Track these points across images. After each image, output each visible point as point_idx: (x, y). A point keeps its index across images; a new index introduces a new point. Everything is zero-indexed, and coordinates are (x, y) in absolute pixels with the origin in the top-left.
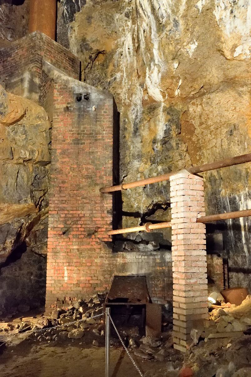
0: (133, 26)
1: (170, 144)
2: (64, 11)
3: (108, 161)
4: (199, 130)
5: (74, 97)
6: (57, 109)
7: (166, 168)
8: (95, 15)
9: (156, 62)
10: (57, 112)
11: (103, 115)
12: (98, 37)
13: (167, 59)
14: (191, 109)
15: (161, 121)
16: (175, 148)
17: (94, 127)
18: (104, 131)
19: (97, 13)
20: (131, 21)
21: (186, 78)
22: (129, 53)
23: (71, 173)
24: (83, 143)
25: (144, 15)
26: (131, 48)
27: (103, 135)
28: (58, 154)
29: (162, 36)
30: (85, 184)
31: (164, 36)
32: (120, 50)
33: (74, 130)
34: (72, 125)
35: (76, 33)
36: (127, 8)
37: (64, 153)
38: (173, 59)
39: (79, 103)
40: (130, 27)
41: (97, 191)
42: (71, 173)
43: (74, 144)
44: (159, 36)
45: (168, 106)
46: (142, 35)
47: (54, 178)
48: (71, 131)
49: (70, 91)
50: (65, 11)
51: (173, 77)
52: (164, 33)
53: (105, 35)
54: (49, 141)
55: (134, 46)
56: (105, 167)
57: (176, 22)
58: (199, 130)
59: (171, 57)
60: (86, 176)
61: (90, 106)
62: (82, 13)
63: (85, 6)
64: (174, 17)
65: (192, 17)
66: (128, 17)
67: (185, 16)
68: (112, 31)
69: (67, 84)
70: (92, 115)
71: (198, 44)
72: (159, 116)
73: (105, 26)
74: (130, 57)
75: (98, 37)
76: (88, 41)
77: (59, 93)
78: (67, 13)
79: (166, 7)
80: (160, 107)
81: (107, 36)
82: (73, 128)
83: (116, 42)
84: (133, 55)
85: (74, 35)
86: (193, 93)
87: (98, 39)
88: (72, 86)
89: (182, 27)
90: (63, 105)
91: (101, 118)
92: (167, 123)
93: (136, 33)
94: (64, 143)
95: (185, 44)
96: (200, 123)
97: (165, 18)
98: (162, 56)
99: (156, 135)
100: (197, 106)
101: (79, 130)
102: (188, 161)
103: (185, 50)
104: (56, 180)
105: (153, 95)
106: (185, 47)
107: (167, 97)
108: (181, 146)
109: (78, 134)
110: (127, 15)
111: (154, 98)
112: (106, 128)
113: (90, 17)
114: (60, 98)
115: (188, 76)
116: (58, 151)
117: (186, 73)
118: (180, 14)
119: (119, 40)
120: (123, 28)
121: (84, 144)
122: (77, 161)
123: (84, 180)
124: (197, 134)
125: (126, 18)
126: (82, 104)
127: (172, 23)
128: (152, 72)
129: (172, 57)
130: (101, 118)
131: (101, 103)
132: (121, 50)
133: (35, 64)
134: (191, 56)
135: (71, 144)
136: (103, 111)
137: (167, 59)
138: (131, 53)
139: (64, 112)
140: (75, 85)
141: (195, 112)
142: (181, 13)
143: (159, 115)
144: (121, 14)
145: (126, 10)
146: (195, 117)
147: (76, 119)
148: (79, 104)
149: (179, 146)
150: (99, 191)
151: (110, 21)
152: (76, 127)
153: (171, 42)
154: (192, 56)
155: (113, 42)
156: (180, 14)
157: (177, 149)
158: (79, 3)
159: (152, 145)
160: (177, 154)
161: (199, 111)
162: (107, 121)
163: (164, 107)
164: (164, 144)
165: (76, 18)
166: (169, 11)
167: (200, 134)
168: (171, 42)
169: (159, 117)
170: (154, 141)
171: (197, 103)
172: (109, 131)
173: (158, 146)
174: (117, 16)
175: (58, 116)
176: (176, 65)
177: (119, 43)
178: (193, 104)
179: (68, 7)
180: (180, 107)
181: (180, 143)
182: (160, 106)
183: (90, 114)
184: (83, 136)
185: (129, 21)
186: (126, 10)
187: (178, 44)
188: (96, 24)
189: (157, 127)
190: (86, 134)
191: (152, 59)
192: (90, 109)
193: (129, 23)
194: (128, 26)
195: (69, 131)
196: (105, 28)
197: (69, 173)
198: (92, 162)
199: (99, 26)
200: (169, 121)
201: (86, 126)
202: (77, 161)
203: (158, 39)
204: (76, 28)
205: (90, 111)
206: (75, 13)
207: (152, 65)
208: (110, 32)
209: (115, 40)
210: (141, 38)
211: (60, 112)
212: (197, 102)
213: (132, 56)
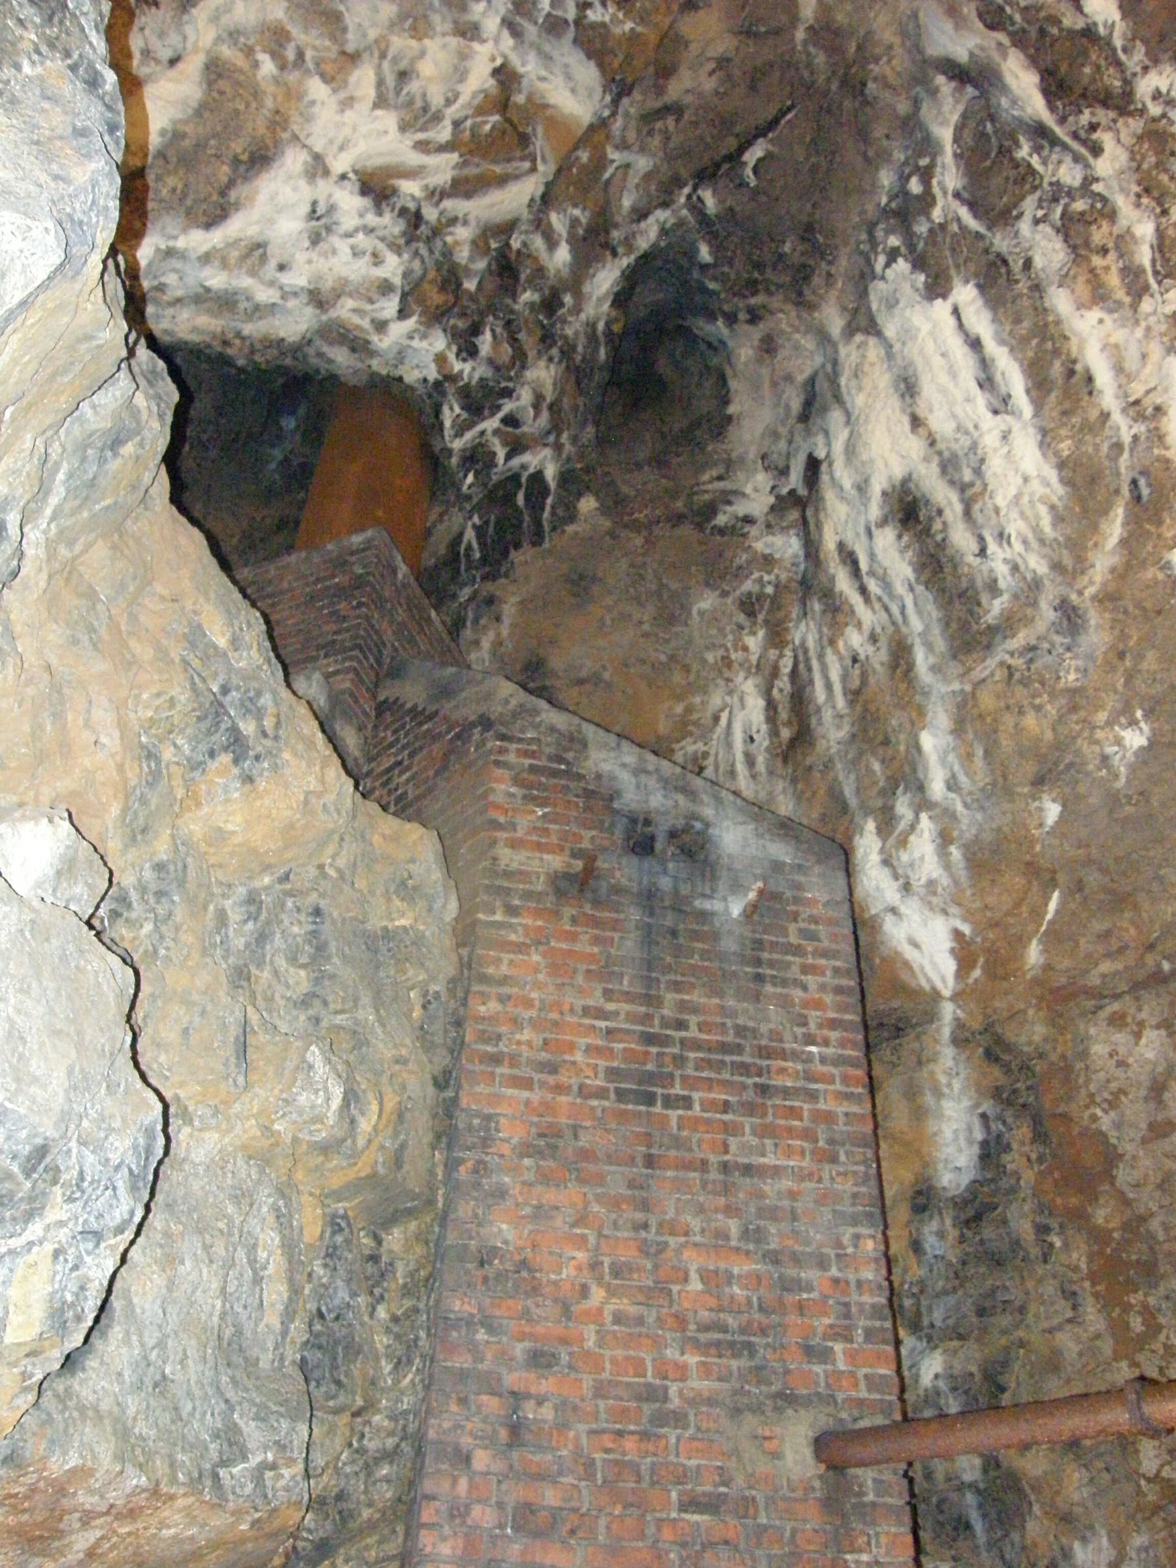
0: (773, 654)
1: (1005, 1222)
2: (461, 535)
3: (857, 1237)
4: (1146, 1162)
5: (613, 825)
6: (508, 874)
7: (973, 1369)
8: (614, 571)
9: (937, 788)
10: (508, 892)
11: (798, 951)
12: (604, 667)
13: (1005, 778)
14: (1099, 1049)
15: (946, 1090)
16: (1035, 1252)
17: (745, 1012)
18: (810, 1040)
19: (624, 564)
20: (761, 633)
21: (1080, 886)
22: (750, 761)
23: (597, 1295)
24: (679, 1098)
25: (856, 599)
26: (763, 740)
27: (812, 1067)
28: (506, 1149)
29: (978, 673)
30: (700, 1385)
31: (992, 674)
32: (691, 749)
33: (617, 1013)
34: (605, 972)
35: (505, 631)
36: (756, 575)
37: (546, 1143)
38: (1039, 782)
39: (648, 863)
40: (754, 659)
41: (795, 1455)
42: (597, 1295)
43: (621, 1095)
44: (963, 675)
45: (976, 1025)
46: (829, 686)
47: (470, 1323)
48: (601, 1014)
49: (589, 794)
50: (470, 535)
51: (1032, 869)
52: (992, 663)
53: (643, 662)
54: (442, 1059)
55: (774, 733)
56: (836, 1281)
57: (1070, 618)
58: (1146, 1162)
59: (1030, 768)
60: (707, 1328)
61: (713, 890)
62: (550, 552)
63: (570, 529)
64: (1063, 590)
65: (1139, 605)
66: (751, 614)
67: (1108, 598)
68: (672, 658)
69: (570, 756)
70: (729, 944)
71: (1152, 730)
72: (931, 1066)
73: (646, 627)
74: (754, 777)
75: (604, 667)
76: (553, 674)
77: (522, 791)
78: (475, 545)
79: (1018, 547)
80: (932, 1021)
81: (647, 669)
82: (608, 994)
83: (679, 709)
84: (771, 773)
85: (491, 635)
86: (1106, 967)
87: (606, 675)
88: (606, 767)
89: (1097, 636)
90: (547, 857)
91: (788, 965)
92: (987, 1106)
93: (783, 683)
94: (551, 1080)
95: (1102, 717)
96: (1151, 1126)
97: (1006, 597)
98: (979, 762)
99: (926, 1165)
100: (1138, 1036)
101: (648, 1017)
102: (1098, 1336)
103: (1097, 749)
104: (481, 1335)
105: (909, 953)
106: (1099, 734)
107: (977, 973)
108: (1066, 1245)
109: (650, 1039)
110: (749, 606)
111: (904, 976)
112: (820, 1026)
113: (582, 577)
114: (529, 818)
115: (1093, 879)
116: (511, 1133)
117: (1090, 861)
118: (1091, 583)
119: (697, 700)
120: (721, 652)
121: (689, 1107)
122: (639, 1216)
123: (692, 1359)
124: (1126, 1189)
125: (741, 618)
126: (665, 872)
127: (1047, 613)
128: (903, 842)
129: (1035, 769)
130: (788, 965)
131: (779, 884)
132: (700, 746)
133: (351, 658)
134: (1123, 780)
135: (601, 1093)
136: (792, 928)
137: (1005, 778)
138: (760, 760)
139: (552, 898)
140: (624, 765)
141: (1122, 1064)
142: (1098, 579)
143: (933, 1060)
144: (724, 594)
145: (748, 586)
146: (1122, 1091)
147: (628, 945)
148: (646, 865)
149: (1051, 1245)
150: (808, 1452)
151: (672, 614)
152: (628, 997)
153: (1038, 701)
154: (1128, 781)
155: (667, 705)
156: (1091, 583)
157: (1045, 1261)
158: (546, 514)
159: (909, 1223)
160: (1050, 1289)
161: (1148, 1061)
162: (823, 987)
163: (959, 1025)
164: (967, 1223)
165: (519, 571)
166: (1037, 564)
167: (1150, 1188)
168: (1038, 701)
169: (932, 1073)
170: (923, 1199)
171: (1143, 1015)
172: (842, 1044)
173: (939, 1238)
174: (706, 602)
175: (512, 911)
176: (1052, 812)
177: (695, 716)
178: (1118, 1021)
179: (487, 523)
180: (1033, 1032)
181: (1054, 1225)
182: (931, 1016)
183: (715, 936)
184: (675, 1057)
185: (754, 634)
186: (748, 586)
187: (1074, 709)
188: (609, 609)
189: (932, 1126)
190: (696, 1045)
191: (906, 775)
192: (715, 905)
193: (754, 642)
194: (745, 649)
195: (586, 1011)
196: (645, 635)
197: (584, 1291)
198: (745, 1234)
199: (625, 617)
200: (997, 1093)
201: (696, 997)
202: (639, 1216)
203: (956, 686)
204: (509, 609)
205: (713, 914)
206: (517, 546)
207: (903, 807)
208: (663, 658)
209: (679, 698)
210: (820, 695)
211: (528, 895)
212: (1140, 1009)
213: (764, 777)
